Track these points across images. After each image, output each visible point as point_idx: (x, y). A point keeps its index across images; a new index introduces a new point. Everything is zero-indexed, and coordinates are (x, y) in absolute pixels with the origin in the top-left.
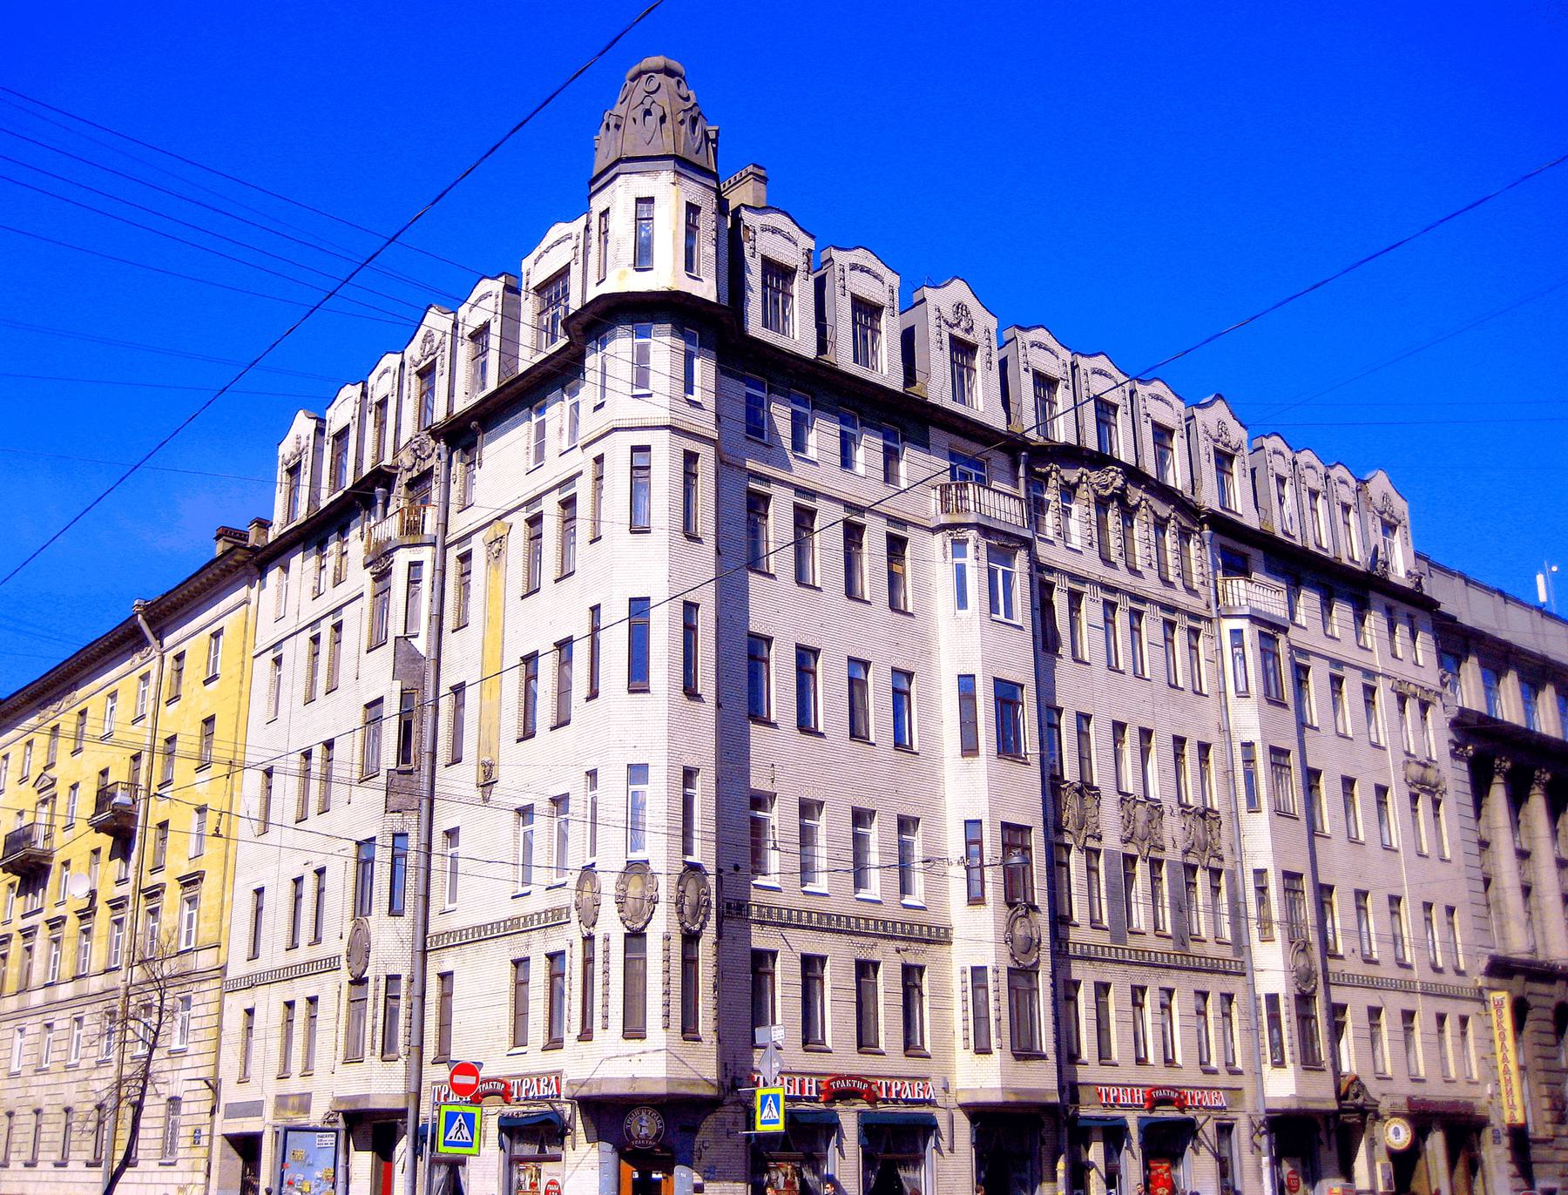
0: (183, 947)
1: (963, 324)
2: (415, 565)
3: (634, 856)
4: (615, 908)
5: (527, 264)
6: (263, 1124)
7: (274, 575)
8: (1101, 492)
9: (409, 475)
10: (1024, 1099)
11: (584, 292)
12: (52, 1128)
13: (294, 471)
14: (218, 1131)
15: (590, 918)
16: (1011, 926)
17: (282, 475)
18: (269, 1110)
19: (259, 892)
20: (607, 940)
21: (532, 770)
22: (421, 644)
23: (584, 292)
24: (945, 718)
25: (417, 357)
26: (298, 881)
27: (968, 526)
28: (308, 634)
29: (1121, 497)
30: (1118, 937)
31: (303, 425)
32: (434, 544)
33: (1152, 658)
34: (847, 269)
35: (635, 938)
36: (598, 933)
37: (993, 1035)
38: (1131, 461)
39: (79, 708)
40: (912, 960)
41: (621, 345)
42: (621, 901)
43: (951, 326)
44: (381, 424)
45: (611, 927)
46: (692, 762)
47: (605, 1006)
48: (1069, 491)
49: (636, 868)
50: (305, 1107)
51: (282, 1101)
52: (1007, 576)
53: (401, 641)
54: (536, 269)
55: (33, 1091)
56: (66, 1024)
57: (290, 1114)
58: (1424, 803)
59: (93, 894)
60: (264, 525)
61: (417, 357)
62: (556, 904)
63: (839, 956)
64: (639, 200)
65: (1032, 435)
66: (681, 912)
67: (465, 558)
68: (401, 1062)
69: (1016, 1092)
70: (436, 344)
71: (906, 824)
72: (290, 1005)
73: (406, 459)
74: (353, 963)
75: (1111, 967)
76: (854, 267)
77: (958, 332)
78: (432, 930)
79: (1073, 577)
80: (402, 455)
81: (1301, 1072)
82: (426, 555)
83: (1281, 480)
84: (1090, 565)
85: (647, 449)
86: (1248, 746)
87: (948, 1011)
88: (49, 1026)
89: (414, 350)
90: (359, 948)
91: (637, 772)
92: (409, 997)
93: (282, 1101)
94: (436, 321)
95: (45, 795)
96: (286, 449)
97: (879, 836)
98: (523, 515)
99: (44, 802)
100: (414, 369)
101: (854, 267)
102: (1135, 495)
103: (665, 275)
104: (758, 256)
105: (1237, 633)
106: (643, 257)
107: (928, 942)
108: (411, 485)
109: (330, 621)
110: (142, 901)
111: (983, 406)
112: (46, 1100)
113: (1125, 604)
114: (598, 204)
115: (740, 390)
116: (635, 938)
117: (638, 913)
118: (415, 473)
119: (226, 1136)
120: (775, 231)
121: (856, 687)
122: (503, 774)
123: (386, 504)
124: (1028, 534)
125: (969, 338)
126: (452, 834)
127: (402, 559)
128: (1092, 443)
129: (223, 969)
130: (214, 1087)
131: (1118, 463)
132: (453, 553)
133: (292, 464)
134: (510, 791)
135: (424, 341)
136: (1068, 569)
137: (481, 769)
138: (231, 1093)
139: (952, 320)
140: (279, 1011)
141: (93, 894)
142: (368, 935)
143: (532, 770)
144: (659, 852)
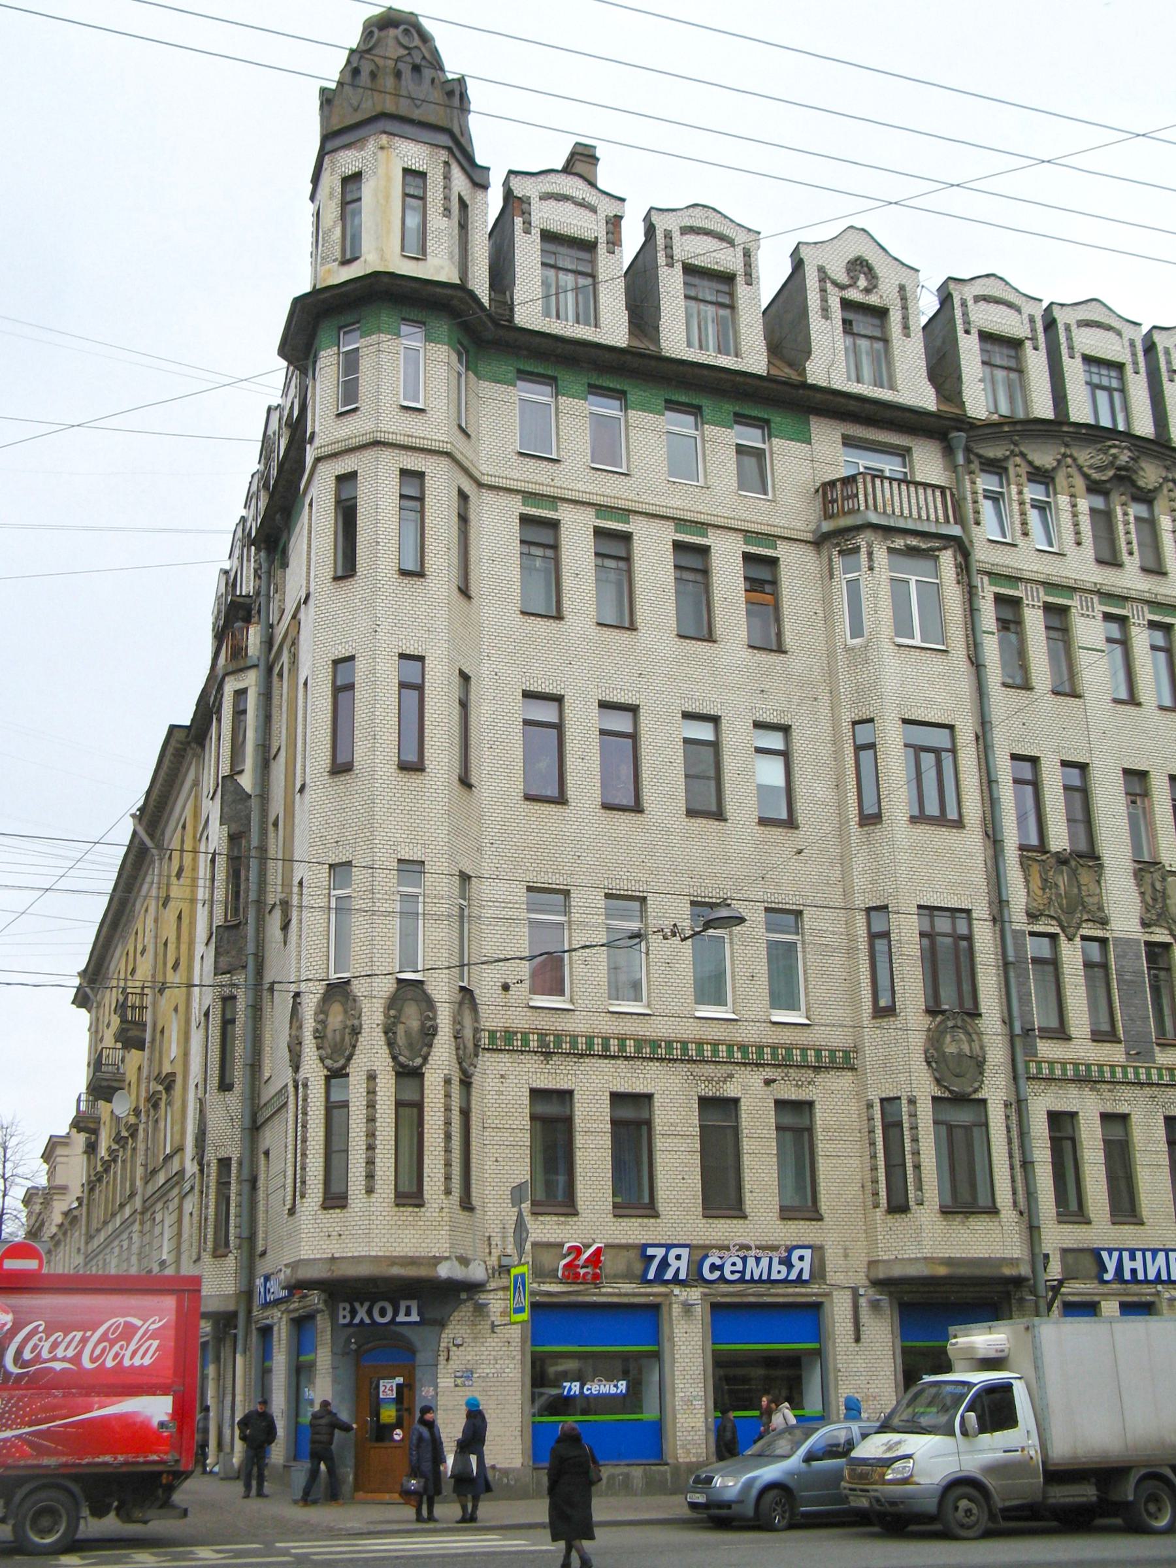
0: (168, 1151)
1: (862, 282)
2: (241, 693)
8: (1096, 476)
10: (962, 1271)
16: (934, 1040)
22: (246, 781)
24: (1129, 883)
29: (1125, 479)
30: (1140, 1052)
34: (676, 235)
37: (911, 1188)
40: (790, 1093)
43: (842, 287)
47: (370, 1162)
49: (338, 991)
53: (229, 783)
68: (231, 1257)
69: (949, 1262)
75: (1128, 1092)
77: (854, 295)
79: (1050, 586)
82: (251, 680)
84: (1081, 566)
85: (352, 476)
87: (844, 1162)
92: (240, 1182)
102: (1150, 474)
104: (536, 232)
107: (817, 1069)
120: (565, 198)
124: (956, 531)
125: (873, 300)
127: (230, 687)
128: (1080, 411)
131: (1128, 435)
136: (1041, 578)
137: (1079, 690)
139: (843, 278)
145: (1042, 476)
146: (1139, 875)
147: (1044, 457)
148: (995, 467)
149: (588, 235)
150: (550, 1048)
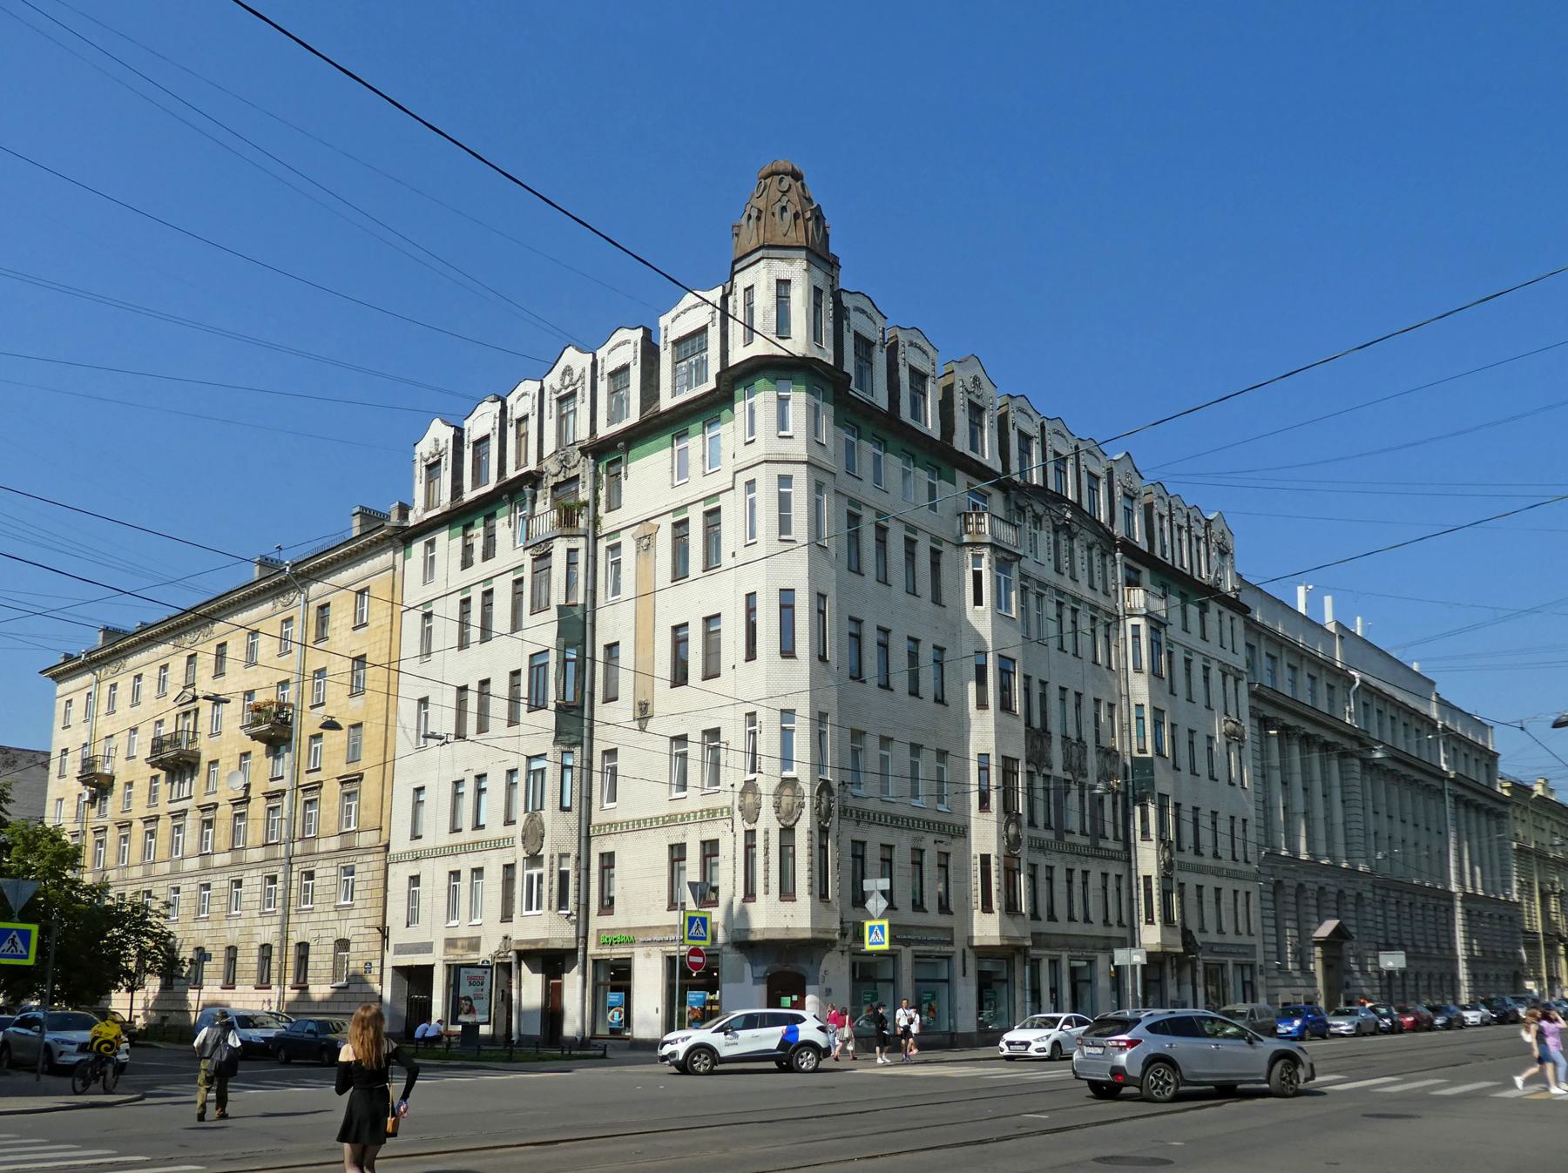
3: (787, 774)
4: (773, 811)
5: (664, 321)
6: (437, 959)
7: (418, 547)
9: (555, 480)
11: (724, 353)
12: (321, 966)
13: (433, 468)
14: (388, 964)
15: (751, 814)
17: (420, 470)
18: (439, 948)
19: (419, 790)
20: (767, 832)
21: (685, 709)
23: (724, 353)
25: (558, 387)
26: (457, 783)
27: (984, 545)
28: (459, 597)
30: (1059, 837)
31: (440, 433)
32: (586, 536)
33: (1085, 641)
35: (787, 832)
36: (760, 828)
38: (1075, 500)
39: (220, 641)
41: (763, 399)
42: (777, 807)
44: (521, 436)
45: (768, 822)
46: (823, 708)
48: (1037, 519)
50: (474, 944)
51: (451, 943)
52: (1007, 582)
54: (674, 325)
55: (195, 934)
56: (226, 884)
57: (459, 952)
58: (1234, 746)
59: (247, 787)
60: (404, 510)
61: (558, 387)
62: (709, 806)
63: (1226, 862)
64: (778, 281)
65: (1017, 478)
66: (819, 815)
67: (615, 548)
70: (575, 377)
71: (942, 754)
72: (455, 875)
73: (551, 466)
74: (528, 844)
76: (857, 309)
78: (594, 821)
80: (546, 463)
81: (1006, 918)
82: (580, 543)
83: (1161, 517)
86: (1140, 706)
88: (207, 887)
89: (553, 380)
90: (534, 835)
91: (787, 714)
93: (451, 943)
94: (574, 359)
95: (185, 708)
96: (424, 448)
97: (927, 763)
98: (670, 520)
99: (186, 714)
100: (555, 396)
101: (857, 309)
103: (798, 343)
105: (1136, 627)
106: (783, 327)
108: (556, 487)
109: (481, 589)
110: (300, 793)
111: (988, 455)
112: (208, 941)
113: (1069, 604)
114: (742, 281)
115: (845, 435)
116: (787, 832)
117: (790, 814)
118: (561, 478)
119: (394, 968)
121: (913, 657)
122: (658, 707)
123: (534, 502)
126: (611, 754)
127: (559, 549)
129: (387, 847)
130: (384, 932)
132: (602, 545)
133: (431, 460)
134: (663, 726)
135: (564, 374)
138: (398, 935)
140: (443, 879)
141: (247, 787)
142: (542, 825)
143: (685, 709)
144: (801, 771)
145: (1037, 519)
146: (1063, 744)
147: (1039, 509)
148: (1021, 510)
149: (872, 338)
150: (861, 817)
